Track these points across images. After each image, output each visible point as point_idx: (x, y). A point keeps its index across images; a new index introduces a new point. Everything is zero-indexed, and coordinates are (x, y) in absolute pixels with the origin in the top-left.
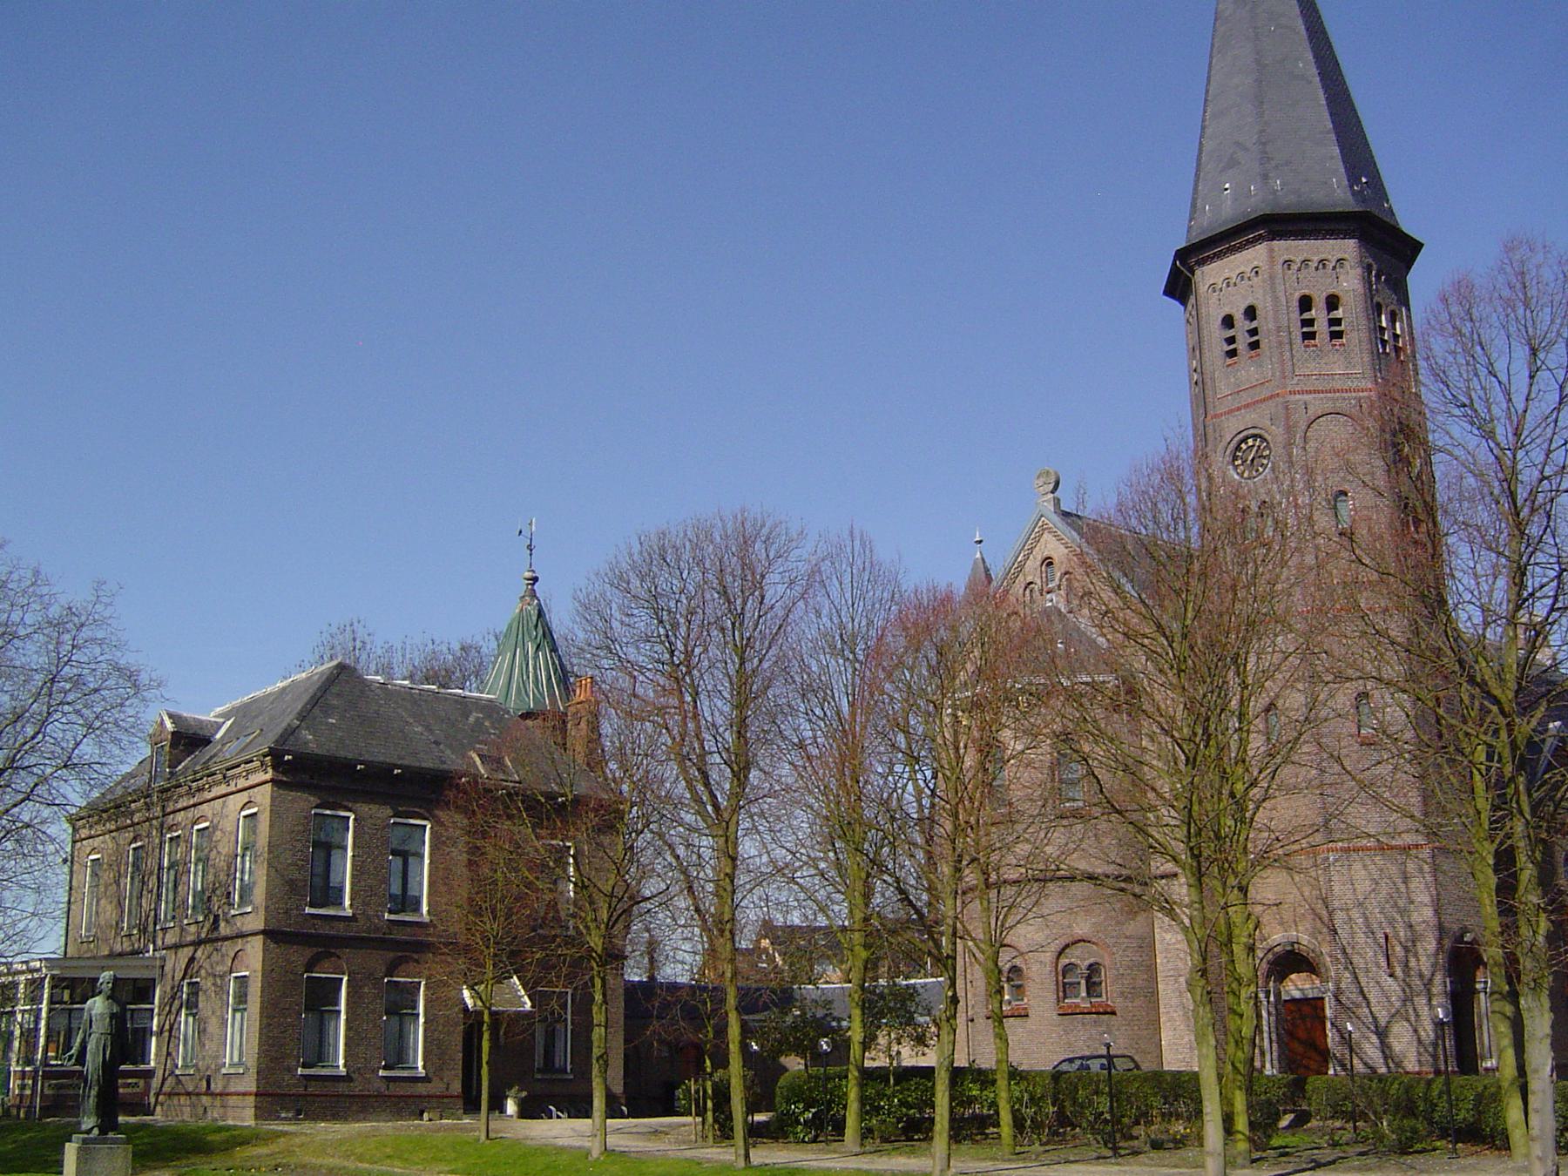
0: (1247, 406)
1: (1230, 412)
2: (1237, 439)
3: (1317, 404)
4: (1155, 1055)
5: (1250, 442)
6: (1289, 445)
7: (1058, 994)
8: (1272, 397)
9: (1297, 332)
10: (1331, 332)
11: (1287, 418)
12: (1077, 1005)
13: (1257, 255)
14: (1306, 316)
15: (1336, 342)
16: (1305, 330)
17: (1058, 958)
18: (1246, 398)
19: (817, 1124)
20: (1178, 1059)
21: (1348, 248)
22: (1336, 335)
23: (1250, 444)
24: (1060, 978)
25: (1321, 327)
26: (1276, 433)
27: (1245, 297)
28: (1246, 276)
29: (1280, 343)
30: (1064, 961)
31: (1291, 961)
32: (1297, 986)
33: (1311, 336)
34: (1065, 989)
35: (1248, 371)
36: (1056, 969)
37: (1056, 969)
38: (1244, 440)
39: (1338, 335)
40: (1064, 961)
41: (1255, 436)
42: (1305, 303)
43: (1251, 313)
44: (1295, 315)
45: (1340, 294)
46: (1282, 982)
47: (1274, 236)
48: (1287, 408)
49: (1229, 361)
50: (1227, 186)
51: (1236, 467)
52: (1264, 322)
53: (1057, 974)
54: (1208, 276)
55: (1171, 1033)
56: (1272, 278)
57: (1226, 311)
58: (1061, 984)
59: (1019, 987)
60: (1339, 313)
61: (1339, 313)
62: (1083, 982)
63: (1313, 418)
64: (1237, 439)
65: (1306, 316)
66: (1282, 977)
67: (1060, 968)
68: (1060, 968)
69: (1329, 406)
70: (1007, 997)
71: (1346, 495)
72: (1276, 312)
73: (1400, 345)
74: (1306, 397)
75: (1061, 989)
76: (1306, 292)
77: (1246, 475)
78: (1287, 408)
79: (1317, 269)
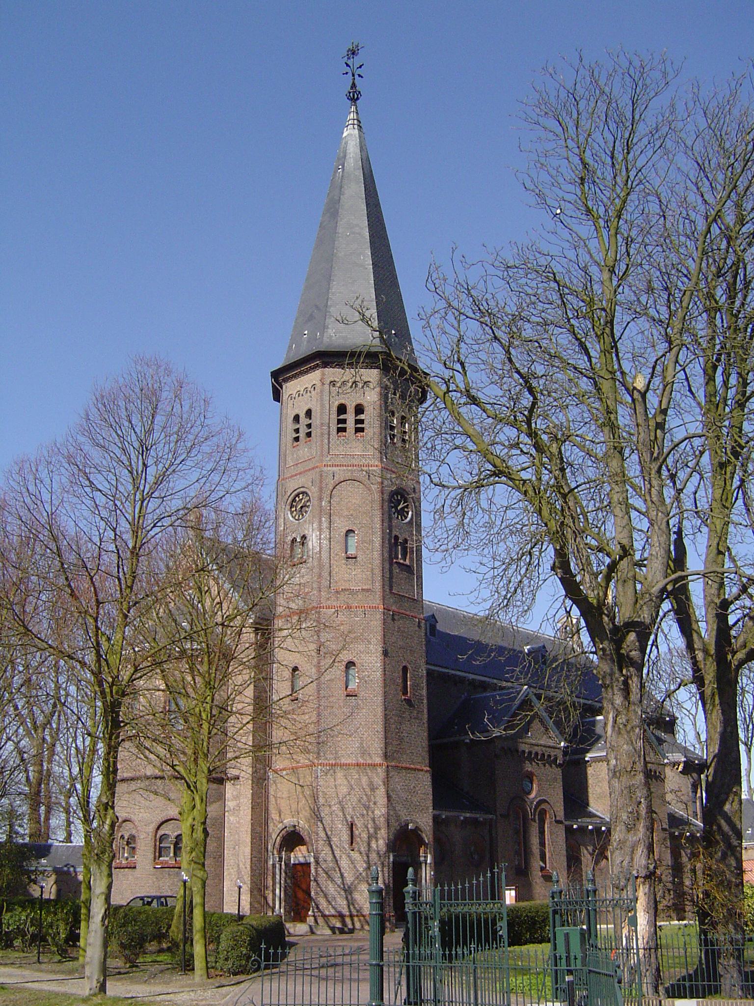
0: (300, 473)
1: (292, 476)
2: (293, 494)
3: (341, 473)
4: (218, 897)
5: (301, 496)
6: (320, 499)
7: (155, 854)
8: (313, 468)
9: (334, 427)
10: (356, 428)
11: (321, 482)
12: (167, 862)
13: (314, 377)
14: (342, 417)
15: (359, 434)
16: (339, 426)
17: (156, 832)
18: (301, 468)
19: (39, 939)
20: (232, 900)
21: (372, 375)
22: (359, 430)
23: (301, 497)
24: (158, 843)
25: (350, 424)
26: (313, 492)
27: (306, 404)
28: (309, 389)
29: (322, 434)
30: (161, 832)
31: (292, 839)
32: (299, 855)
33: (344, 430)
34: (160, 852)
35: (304, 451)
36: (156, 836)
37: (156, 836)
38: (298, 495)
39: (362, 430)
40: (161, 832)
41: (303, 493)
42: (342, 409)
43: (309, 413)
44: (334, 417)
45: (365, 404)
46: (292, 851)
47: (325, 365)
48: (321, 476)
49: (296, 444)
50: (306, 332)
51: (292, 513)
52: (316, 420)
53: (156, 840)
54: (290, 388)
55: (229, 883)
56: (322, 392)
57: (296, 412)
58: (158, 848)
59: (134, 848)
60: (362, 417)
61: (362, 417)
62: (172, 846)
63: (337, 483)
64: (293, 494)
65: (342, 417)
66: (291, 849)
67: (158, 836)
68: (158, 836)
69: (348, 475)
70: (126, 855)
71: (354, 532)
72: (322, 413)
73: (407, 438)
74: (334, 468)
75: (157, 851)
76: (343, 402)
77: (297, 518)
78: (321, 476)
79: (351, 387)
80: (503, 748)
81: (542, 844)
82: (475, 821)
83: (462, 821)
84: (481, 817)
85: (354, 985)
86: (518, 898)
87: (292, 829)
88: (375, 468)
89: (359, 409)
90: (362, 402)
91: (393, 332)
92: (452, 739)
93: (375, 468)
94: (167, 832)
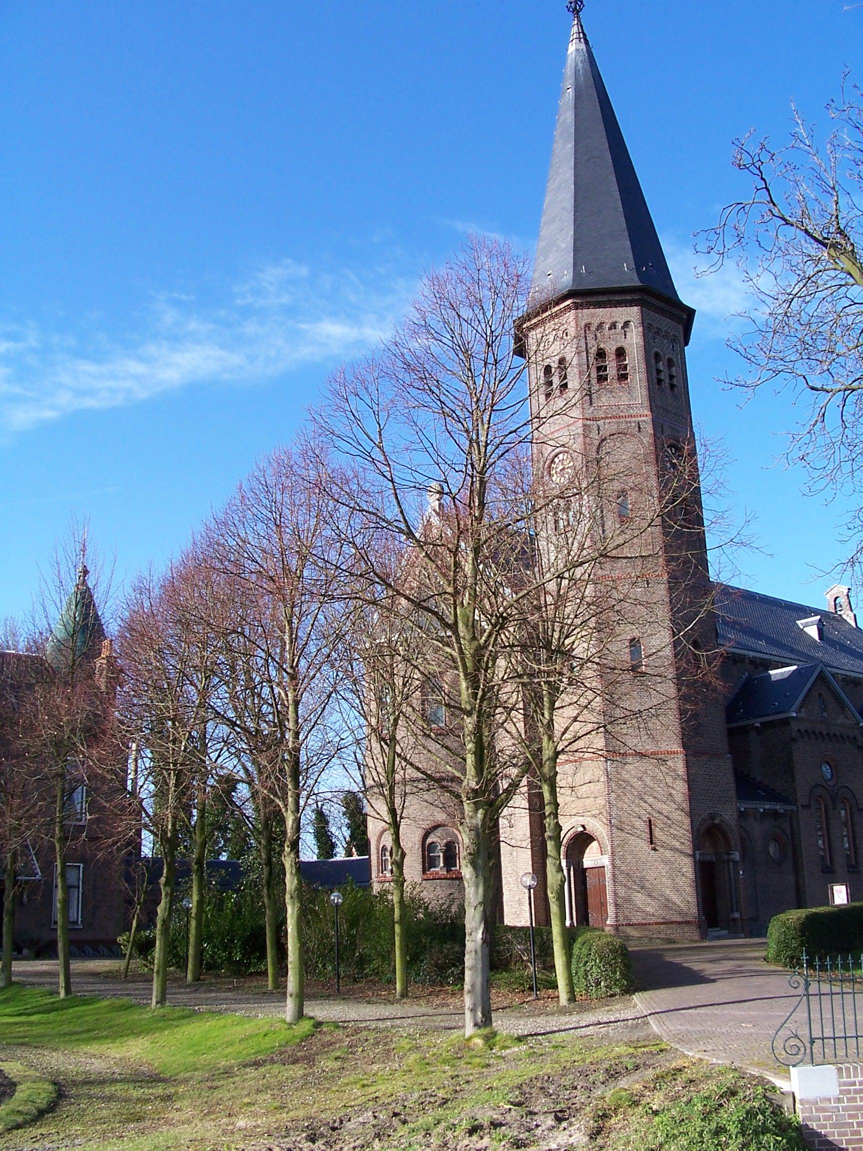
12: (437, 873)
20: (512, 912)
21: (633, 313)
25: (612, 371)
30: (429, 841)
40: (429, 841)
62: (441, 855)
80: (799, 730)
81: (530, 898)
82: (775, 815)
83: (762, 813)
84: (779, 807)
85: (826, 1000)
86: (851, 896)
87: (581, 829)
88: (645, 418)
89: (621, 353)
90: (624, 345)
91: (650, 264)
92: (739, 724)
93: (645, 418)
94: (435, 840)
